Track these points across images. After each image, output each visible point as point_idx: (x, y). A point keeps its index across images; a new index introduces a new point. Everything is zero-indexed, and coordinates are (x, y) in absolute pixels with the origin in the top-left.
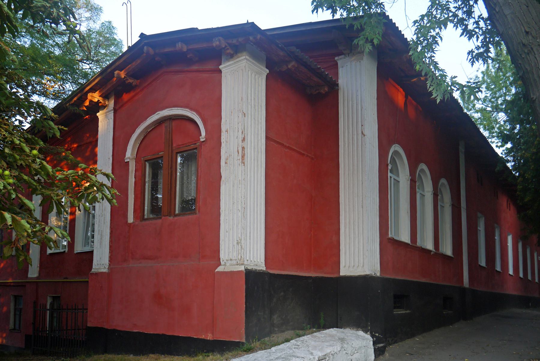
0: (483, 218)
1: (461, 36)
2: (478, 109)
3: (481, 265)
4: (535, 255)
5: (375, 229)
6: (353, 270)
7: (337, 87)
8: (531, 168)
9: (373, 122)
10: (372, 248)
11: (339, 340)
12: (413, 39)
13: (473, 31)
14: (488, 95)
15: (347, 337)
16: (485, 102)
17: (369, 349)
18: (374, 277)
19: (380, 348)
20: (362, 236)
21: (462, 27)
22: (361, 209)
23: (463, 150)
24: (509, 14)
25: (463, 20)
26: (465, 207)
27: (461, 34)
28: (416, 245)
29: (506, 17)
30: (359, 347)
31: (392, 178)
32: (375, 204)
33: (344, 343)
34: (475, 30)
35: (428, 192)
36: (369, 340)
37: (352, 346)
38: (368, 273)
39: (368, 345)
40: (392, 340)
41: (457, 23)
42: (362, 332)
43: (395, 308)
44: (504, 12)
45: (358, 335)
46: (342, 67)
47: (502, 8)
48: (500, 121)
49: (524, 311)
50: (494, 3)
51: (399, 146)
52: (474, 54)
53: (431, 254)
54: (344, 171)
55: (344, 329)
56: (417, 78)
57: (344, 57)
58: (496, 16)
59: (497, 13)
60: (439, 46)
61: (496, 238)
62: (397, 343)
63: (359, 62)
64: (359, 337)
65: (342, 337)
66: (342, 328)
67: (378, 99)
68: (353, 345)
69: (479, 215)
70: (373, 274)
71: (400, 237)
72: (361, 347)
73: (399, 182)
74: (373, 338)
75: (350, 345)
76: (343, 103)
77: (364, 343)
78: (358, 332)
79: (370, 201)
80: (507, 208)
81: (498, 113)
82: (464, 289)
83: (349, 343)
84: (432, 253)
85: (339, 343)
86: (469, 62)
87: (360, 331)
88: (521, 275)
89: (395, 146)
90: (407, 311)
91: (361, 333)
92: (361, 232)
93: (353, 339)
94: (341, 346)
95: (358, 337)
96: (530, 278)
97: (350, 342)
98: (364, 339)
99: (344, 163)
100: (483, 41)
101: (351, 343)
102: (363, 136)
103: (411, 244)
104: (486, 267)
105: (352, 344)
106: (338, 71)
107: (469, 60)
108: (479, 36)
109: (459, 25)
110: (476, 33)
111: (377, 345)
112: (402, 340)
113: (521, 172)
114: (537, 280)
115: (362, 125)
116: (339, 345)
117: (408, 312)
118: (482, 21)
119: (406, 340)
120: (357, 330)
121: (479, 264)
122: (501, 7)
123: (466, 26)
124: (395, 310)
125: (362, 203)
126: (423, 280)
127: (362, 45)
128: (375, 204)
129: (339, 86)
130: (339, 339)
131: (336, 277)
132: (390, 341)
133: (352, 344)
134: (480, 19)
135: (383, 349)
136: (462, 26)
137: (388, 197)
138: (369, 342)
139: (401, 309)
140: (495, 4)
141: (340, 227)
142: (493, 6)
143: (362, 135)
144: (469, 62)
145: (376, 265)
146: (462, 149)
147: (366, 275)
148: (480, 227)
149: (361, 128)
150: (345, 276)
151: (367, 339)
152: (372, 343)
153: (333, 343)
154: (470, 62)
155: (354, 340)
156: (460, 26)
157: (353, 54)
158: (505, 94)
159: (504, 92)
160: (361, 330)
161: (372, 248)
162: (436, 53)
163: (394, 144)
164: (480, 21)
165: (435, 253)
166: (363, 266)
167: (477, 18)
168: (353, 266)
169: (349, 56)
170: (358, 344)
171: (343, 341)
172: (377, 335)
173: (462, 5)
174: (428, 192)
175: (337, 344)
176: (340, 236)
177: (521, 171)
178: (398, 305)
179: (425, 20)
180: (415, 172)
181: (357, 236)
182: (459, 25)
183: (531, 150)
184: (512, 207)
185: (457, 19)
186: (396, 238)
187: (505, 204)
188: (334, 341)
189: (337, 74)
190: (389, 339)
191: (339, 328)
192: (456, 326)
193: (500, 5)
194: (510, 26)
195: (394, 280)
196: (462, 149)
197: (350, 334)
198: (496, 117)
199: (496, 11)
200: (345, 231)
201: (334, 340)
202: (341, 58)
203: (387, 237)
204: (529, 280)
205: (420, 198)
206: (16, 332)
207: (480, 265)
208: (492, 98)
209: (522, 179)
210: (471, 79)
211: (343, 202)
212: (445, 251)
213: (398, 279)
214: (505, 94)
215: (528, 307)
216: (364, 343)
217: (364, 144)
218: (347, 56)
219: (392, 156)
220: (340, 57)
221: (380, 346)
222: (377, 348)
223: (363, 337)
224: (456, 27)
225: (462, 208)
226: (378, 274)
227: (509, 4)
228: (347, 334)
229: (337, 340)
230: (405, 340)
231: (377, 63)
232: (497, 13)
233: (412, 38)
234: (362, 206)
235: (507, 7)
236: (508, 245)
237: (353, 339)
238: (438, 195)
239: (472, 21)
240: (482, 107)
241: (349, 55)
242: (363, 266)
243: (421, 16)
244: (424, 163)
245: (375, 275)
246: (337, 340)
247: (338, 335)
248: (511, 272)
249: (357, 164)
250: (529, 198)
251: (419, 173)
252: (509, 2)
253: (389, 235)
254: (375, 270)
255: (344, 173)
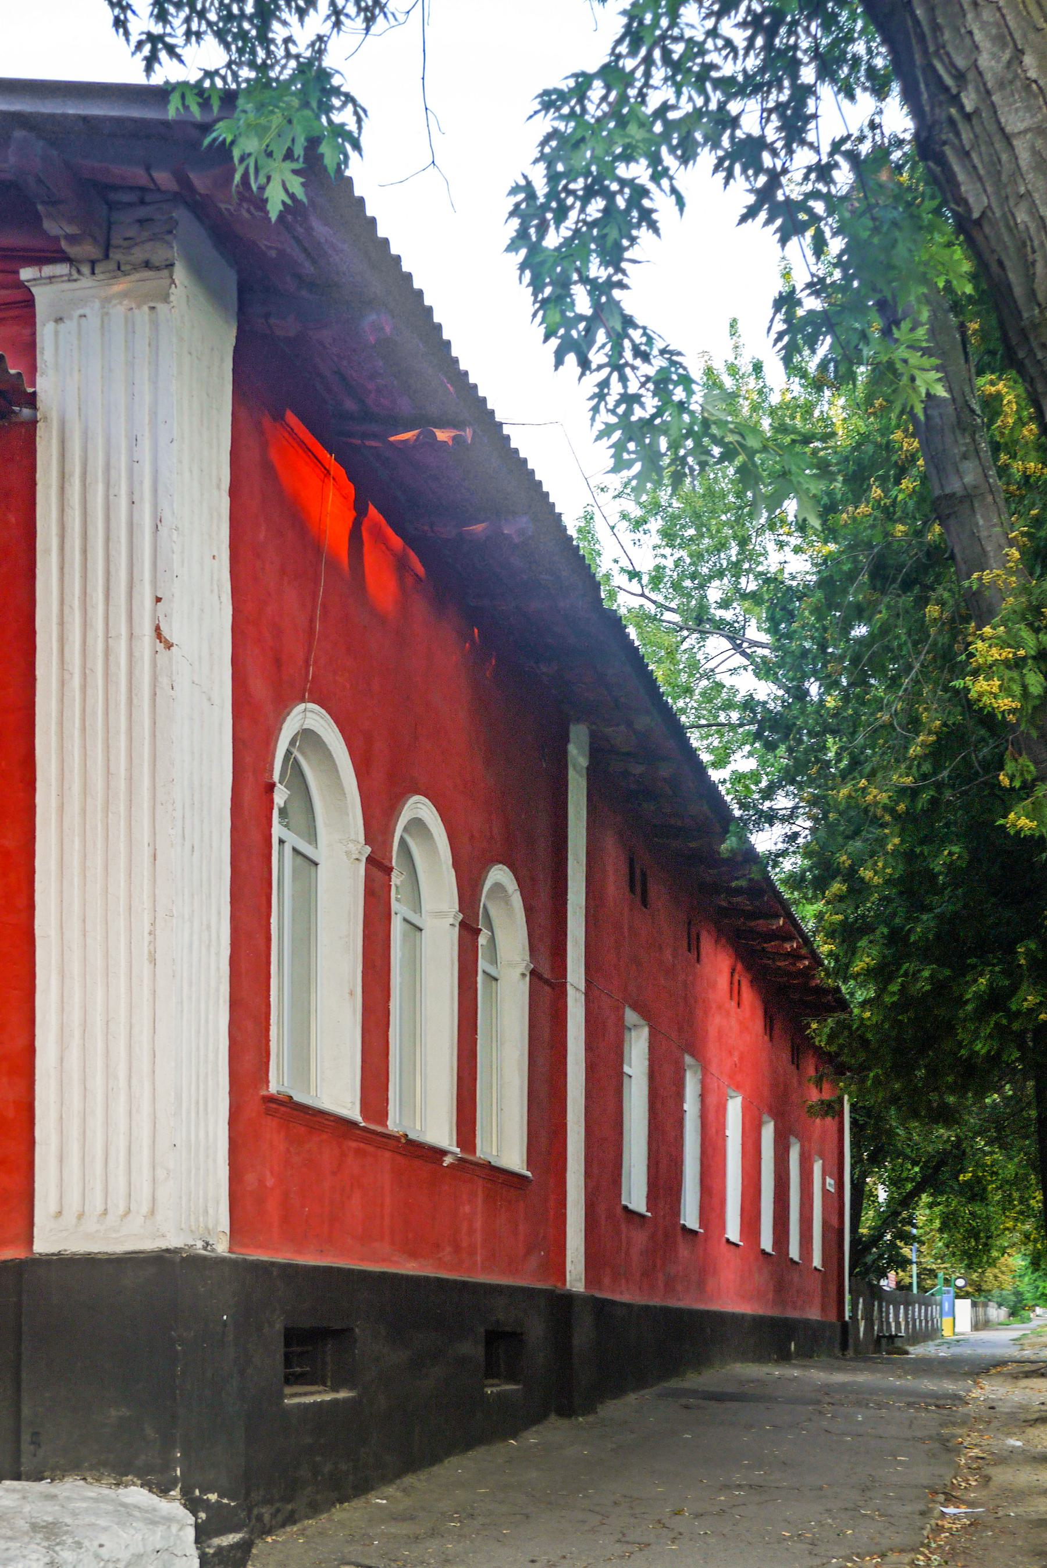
0: (646, 1031)
1: (744, 219)
2: (629, 611)
3: (631, 1207)
4: (817, 1167)
5: (211, 1056)
6: (97, 1231)
7: (26, 412)
8: (890, 847)
9: (212, 591)
10: (197, 1136)
11: (34, 1531)
12: (529, 184)
13: (802, 206)
14: (669, 563)
15: (74, 1514)
16: (656, 588)
17: (177, 1561)
18: (204, 1258)
19: (225, 1553)
20: (147, 1084)
21: (752, 179)
22: (147, 967)
23: (583, 762)
24: (1025, 132)
25: (755, 146)
26: (582, 986)
27: (745, 211)
28: (387, 1126)
29: (1010, 145)
30: (133, 1555)
31: (286, 845)
32: (213, 951)
33: (58, 1544)
34: (811, 203)
35: (439, 914)
36: (178, 1522)
37: (97, 1556)
38: (173, 1240)
39: (175, 1544)
40: (274, 1516)
41: (733, 156)
42: (144, 1491)
43: (290, 1379)
44: (1003, 120)
45: (124, 1505)
46: (59, 320)
47: (994, 98)
48: (712, 670)
49: (777, 1371)
50: (953, 71)
51: (323, 711)
52: (800, 312)
53: (445, 1164)
54: (61, 795)
55: (53, 1480)
56: (416, 432)
57: (70, 274)
58: (958, 134)
59: (968, 117)
60: (656, 231)
61: (686, 1107)
62: (295, 1523)
63: (145, 308)
64: (129, 1515)
65: (50, 1519)
66: (41, 1479)
67: (234, 492)
68: (103, 1552)
69: (631, 1016)
70: (200, 1244)
71: (313, 1093)
72: (140, 1556)
73: (316, 864)
74: (194, 1513)
75: (87, 1550)
76: (62, 489)
77: (156, 1538)
78: (121, 1491)
79: (191, 934)
80: (731, 998)
81: (704, 634)
82: (568, 1299)
83: (86, 1543)
84: (448, 1160)
85: (35, 1547)
86: (775, 345)
87: (134, 1484)
88: (767, 1243)
89: (305, 710)
90: (338, 1391)
91: (137, 1495)
92: (146, 1067)
93: (102, 1522)
94: (47, 1560)
95: (126, 1513)
96: (794, 1253)
97: (87, 1537)
98: (153, 1520)
99: (62, 761)
100: (845, 258)
101: (96, 1544)
102: (160, 646)
103: (363, 1124)
104: (649, 1214)
105: (101, 1546)
106: (34, 334)
107: (773, 335)
108: (828, 234)
109: (737, 168)
110: (815, 219)
111: (210, 1538)
112: (315, 1509)
113: (844, 862)
114: (817, 1262)
115: (158, 600)
116: (34, 1556)
117: (343, 1394)
118: (845, 165)
119: (333, 1510)
120: (118, 1485)
121: (624, 1203)
122: (988, 93)
123: (775, 178)
124: (288, 1390)
125: (153, 942)
126: (410, 1268)
127: (251, 162)
128: (213, 951)
129: (39, 404)
130: (35, 1527)
131: (12, 1260)
132: (267, 1518)
133: (101, 1546)
134: (838, 157)
135: (239, 1555)
136: (750, 172)
137: (269, 924)
138: (180, 1530)
139: (312, 1384)
140: (960, 77)
141: (38, 1044)
142: (949, 81)
143: (155, 645)
144: (775, 345)
145: (211, 1211)
146: (578, 757)
147: (167, 1250)
148: (630, 1067)
149: (155, 611)
150: (59, 1253)
151: (168, 1520)
152: (190, 1533)
153: (7, 1549)
154: (780, 345)
155: (105, 1529)
156: (744, 171)
157: (119, 268)
158: (737, 565)
159: (734, 559)
160: (139, 1482)
161: (197, 1136)
162: (628, 272)
163: (303, 700)
164: (836, 165)
165: (461, 1159)
166: (152, 1212)
167: (825, 148)
168: (100, 1208)
169: (93, 273)
170: (127, 1547)
171: (57, 1535)
172: (213, 1497)
173: (762, 70)
174: (439, 914)
175: (25, 1552)
176: (37, 1083)
177: (845, 858)
178: (298, 1369)
179: (592, 102)
180: (388, 831)
181: (123, 1083)
182: (737, 168)
183: (895, 777)
184: (748, 995)
185: (732, 137)
186: (299, 1097)
187: (723, 982)
188: (11, 1539)
189: (29, 348)
190: (263, 1510)
191: (28, 1480)
192: (532, 1438)
193: (985, 84)
194: (1022, 190)
195: (290, 1272)
196: (578, 757)
197: (84, 1505)
198: (695, 650)
199: (961, 107)
200: (62, 1059)
201: (9, 1533)
202: (50, 278)
203: (264, 1093)
204: (792, 1259)
205: (405, 936)
206: (312, 621)
207: (626, 1208)
208: (682, 577)
209: (844, 888)
210: (602, 490)
211: (53, 933)
212: (494, 1153)
213: (305, 1268)
214: (736, 570)
215: (784, 1357)
216: (156, 1538)
217: (164, 681)
218: (86, 269)
219: (289, 753)
220: (48, 270)
221: (225, 1544)
222: (211, 1551)
223: (147, 1511)
224: (724, 174)
225: (569, 989)
226: (222, 1247)
227: (1029, 86)
228: (71, 1506)
229: (26, 1533)
230: (329, 1510)
231: (234, 332)
232: (968, 117)
233: (525, 177)
234: (150, 953)
235: (1017, 97)
236: (728, 1133)
237: (102, 1522)
238: (478, 931)
239: (804, 158)
240: (642, 606)
241: (96, 272)
242: (152, 1212)
243: (576, 76)
244: (426, 796)
245: (205, 1248)
246: (26, 1533)
247: (27, 1509)
248: (733, 1231)
249: (130, 769)
250: (867, 960)
251: (402, 839)
252: (1028, 79)
253: (271, 1085)
254: (207, 1229)
255: (61, 808)
